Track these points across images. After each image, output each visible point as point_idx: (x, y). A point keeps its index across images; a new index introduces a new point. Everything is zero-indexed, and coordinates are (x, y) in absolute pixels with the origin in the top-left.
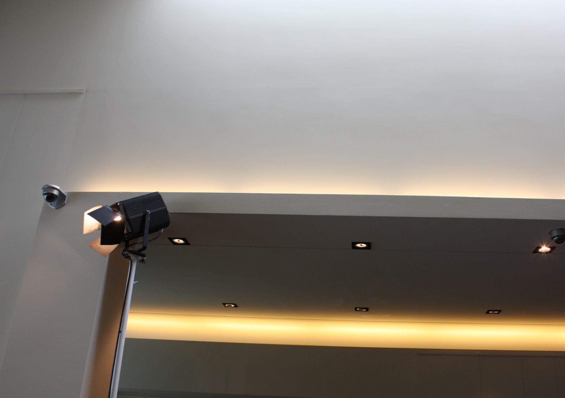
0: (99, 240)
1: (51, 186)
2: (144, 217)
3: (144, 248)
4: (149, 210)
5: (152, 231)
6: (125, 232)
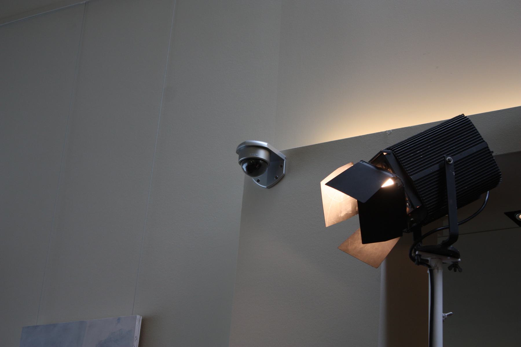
0: (359, 236)
1: (252, 142)
2: (442, 173)
3: (453, 238)
4: (451, 156)
5: (462, 201)
6: (408, 209)
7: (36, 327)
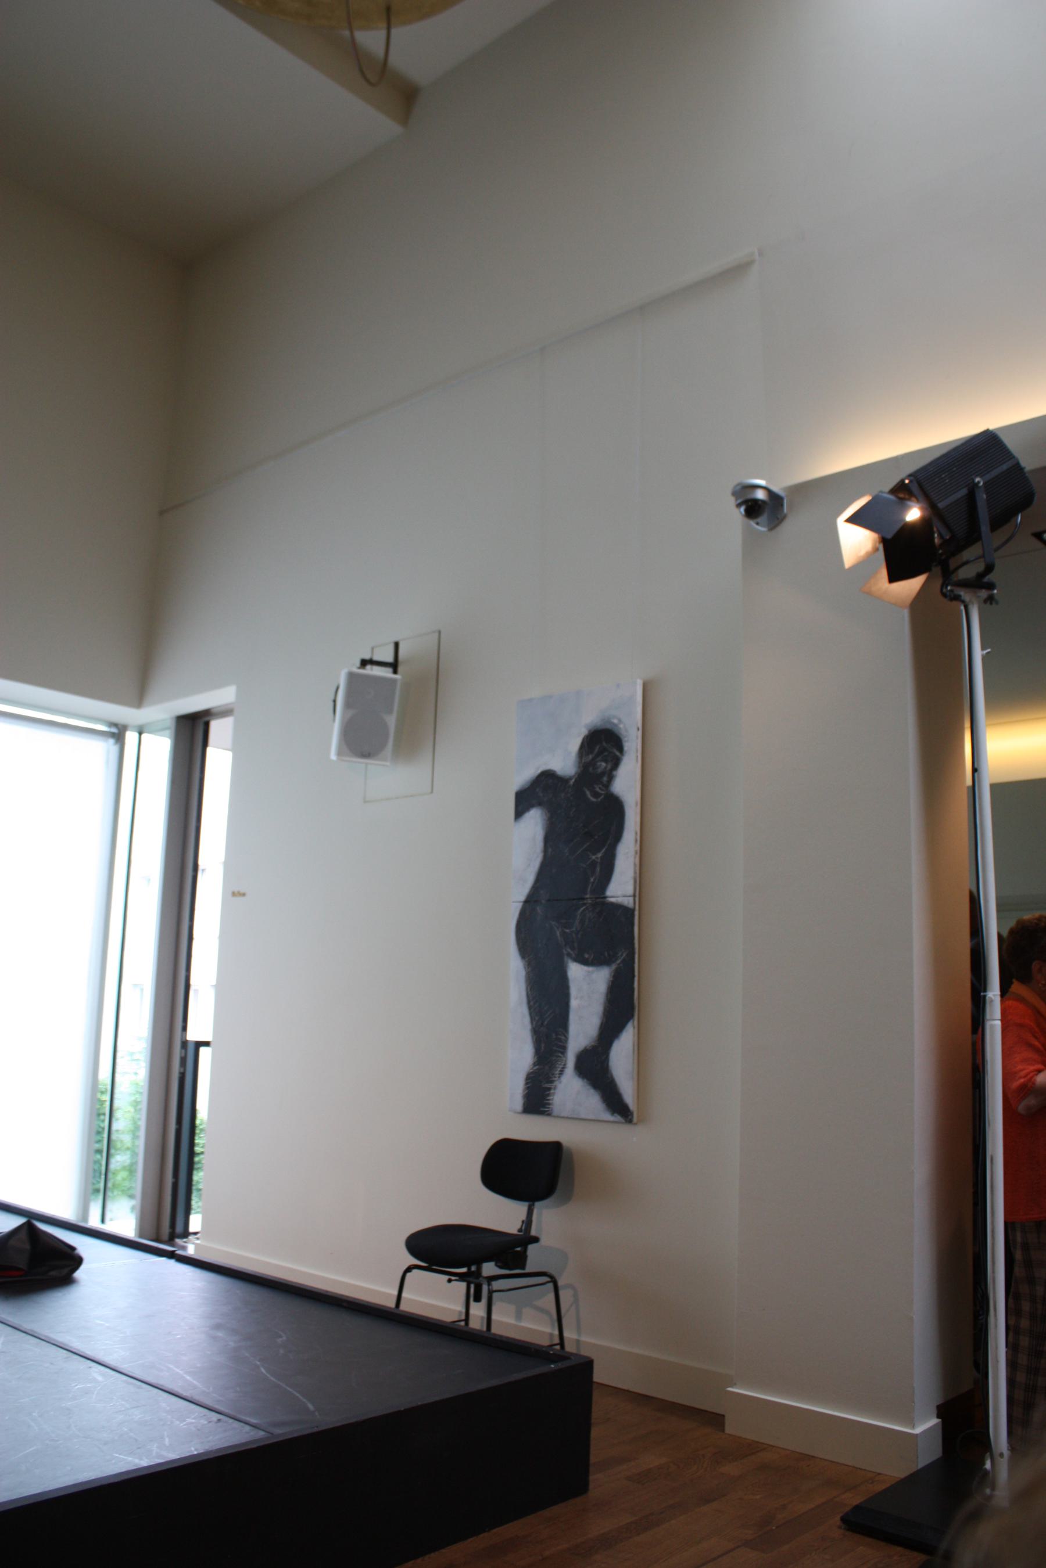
0: (884, 573)
3: (989, 568)
4: (981, 477)
7: (531, 700)
